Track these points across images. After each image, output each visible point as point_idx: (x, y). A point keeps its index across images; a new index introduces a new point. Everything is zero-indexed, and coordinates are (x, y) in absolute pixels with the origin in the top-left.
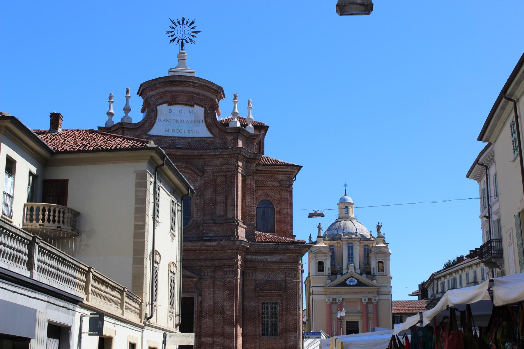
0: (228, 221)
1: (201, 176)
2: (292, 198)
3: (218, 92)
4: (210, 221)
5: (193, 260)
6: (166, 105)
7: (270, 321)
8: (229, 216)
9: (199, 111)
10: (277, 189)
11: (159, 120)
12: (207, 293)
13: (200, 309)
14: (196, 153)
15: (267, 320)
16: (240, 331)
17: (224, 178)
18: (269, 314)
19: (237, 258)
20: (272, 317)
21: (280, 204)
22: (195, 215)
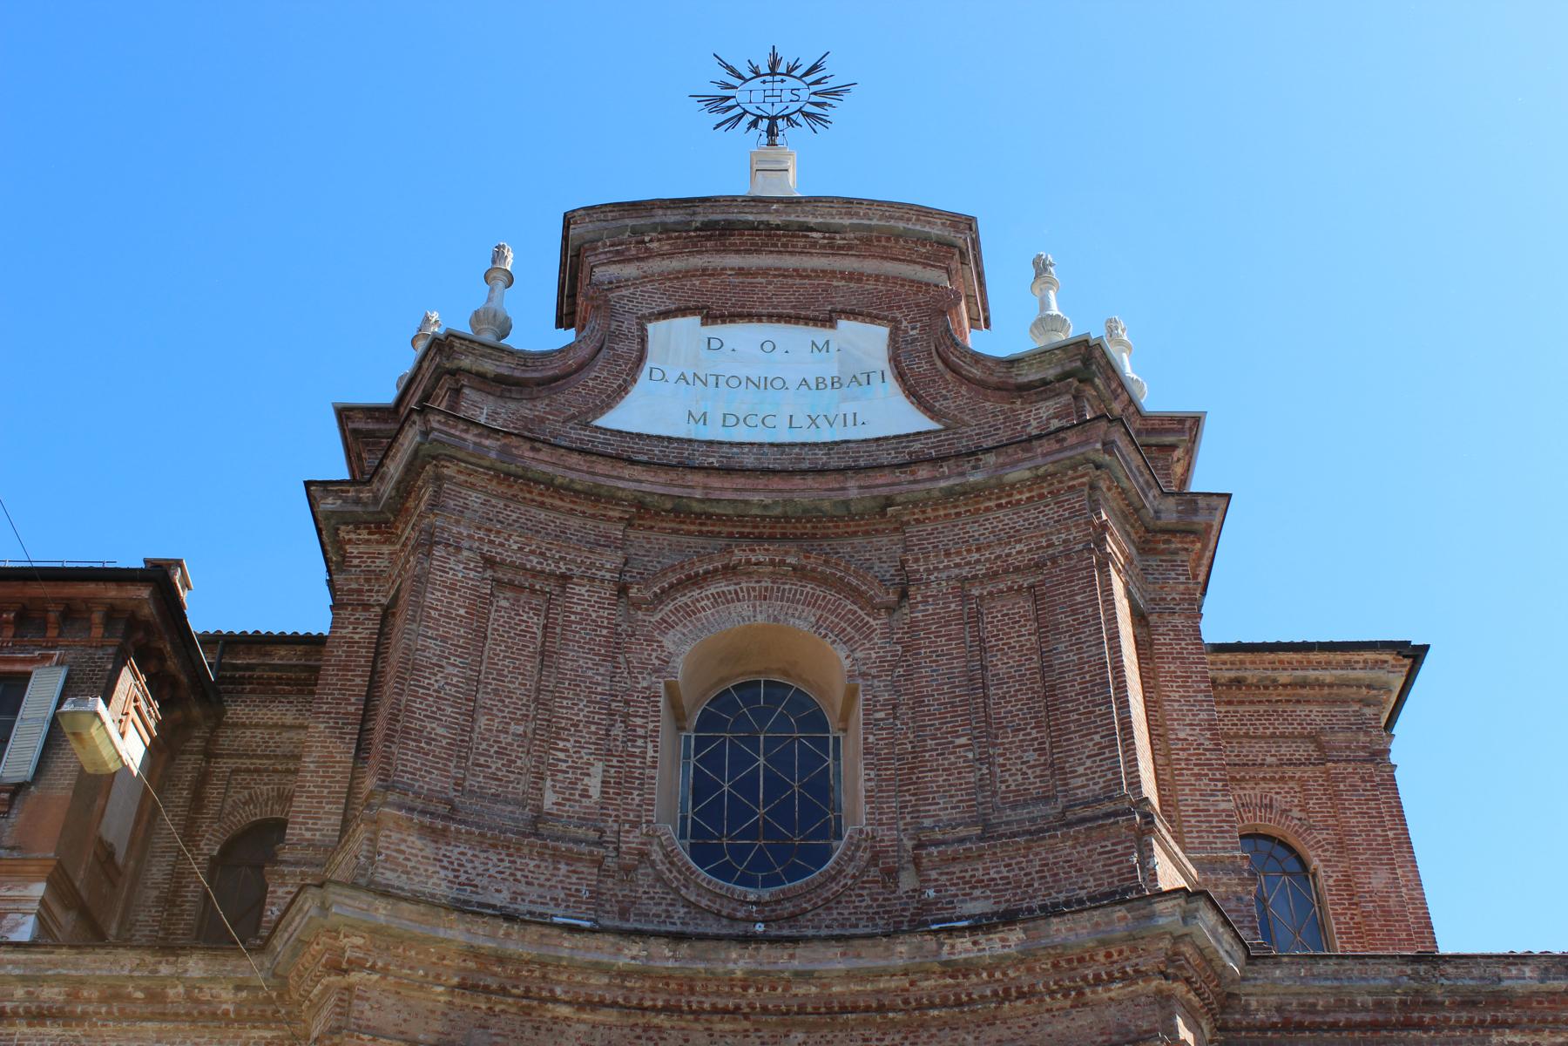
0: (1081, 812)
1: (890, 609)
2: (1401, 816)
3: (951, 243)
4: (962, 832)
6: (697, 319)
8: (1084, 781)
9: (865, 342)
10: (1309, 772)
11: (657, 375)
14: (853, 489)
17: (1024, 605)
22: (863, 809)
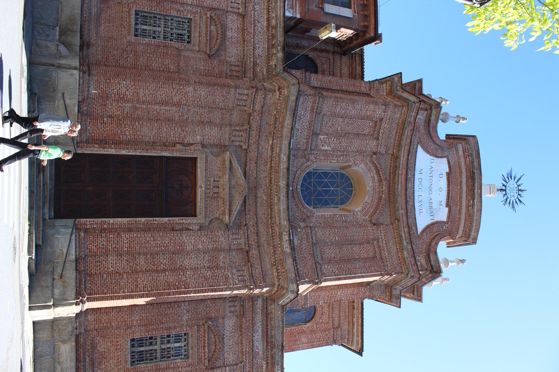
0: (318, 267)
1: (371, 221)
2: (319, 346)
3: (469, 238)
4: (314, 238)
5: (256, 214)
7: (156, 347)
8: (326, 268)
9: (442, 215)
10: (331, 324)
11: (432, 161)
12: (204, 239)
13: (177, 227)
14: (402, 212)
15: (158, 343)
16: (141, 301)
17: (371, 255)
18: (169, 346)
19: (266, 287)
20: (163, 350)
21: (312, 331)
22: (320, 214)
